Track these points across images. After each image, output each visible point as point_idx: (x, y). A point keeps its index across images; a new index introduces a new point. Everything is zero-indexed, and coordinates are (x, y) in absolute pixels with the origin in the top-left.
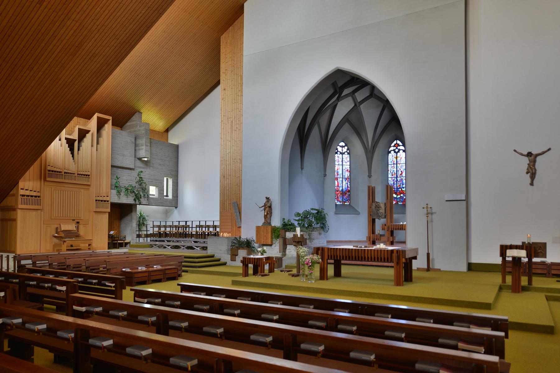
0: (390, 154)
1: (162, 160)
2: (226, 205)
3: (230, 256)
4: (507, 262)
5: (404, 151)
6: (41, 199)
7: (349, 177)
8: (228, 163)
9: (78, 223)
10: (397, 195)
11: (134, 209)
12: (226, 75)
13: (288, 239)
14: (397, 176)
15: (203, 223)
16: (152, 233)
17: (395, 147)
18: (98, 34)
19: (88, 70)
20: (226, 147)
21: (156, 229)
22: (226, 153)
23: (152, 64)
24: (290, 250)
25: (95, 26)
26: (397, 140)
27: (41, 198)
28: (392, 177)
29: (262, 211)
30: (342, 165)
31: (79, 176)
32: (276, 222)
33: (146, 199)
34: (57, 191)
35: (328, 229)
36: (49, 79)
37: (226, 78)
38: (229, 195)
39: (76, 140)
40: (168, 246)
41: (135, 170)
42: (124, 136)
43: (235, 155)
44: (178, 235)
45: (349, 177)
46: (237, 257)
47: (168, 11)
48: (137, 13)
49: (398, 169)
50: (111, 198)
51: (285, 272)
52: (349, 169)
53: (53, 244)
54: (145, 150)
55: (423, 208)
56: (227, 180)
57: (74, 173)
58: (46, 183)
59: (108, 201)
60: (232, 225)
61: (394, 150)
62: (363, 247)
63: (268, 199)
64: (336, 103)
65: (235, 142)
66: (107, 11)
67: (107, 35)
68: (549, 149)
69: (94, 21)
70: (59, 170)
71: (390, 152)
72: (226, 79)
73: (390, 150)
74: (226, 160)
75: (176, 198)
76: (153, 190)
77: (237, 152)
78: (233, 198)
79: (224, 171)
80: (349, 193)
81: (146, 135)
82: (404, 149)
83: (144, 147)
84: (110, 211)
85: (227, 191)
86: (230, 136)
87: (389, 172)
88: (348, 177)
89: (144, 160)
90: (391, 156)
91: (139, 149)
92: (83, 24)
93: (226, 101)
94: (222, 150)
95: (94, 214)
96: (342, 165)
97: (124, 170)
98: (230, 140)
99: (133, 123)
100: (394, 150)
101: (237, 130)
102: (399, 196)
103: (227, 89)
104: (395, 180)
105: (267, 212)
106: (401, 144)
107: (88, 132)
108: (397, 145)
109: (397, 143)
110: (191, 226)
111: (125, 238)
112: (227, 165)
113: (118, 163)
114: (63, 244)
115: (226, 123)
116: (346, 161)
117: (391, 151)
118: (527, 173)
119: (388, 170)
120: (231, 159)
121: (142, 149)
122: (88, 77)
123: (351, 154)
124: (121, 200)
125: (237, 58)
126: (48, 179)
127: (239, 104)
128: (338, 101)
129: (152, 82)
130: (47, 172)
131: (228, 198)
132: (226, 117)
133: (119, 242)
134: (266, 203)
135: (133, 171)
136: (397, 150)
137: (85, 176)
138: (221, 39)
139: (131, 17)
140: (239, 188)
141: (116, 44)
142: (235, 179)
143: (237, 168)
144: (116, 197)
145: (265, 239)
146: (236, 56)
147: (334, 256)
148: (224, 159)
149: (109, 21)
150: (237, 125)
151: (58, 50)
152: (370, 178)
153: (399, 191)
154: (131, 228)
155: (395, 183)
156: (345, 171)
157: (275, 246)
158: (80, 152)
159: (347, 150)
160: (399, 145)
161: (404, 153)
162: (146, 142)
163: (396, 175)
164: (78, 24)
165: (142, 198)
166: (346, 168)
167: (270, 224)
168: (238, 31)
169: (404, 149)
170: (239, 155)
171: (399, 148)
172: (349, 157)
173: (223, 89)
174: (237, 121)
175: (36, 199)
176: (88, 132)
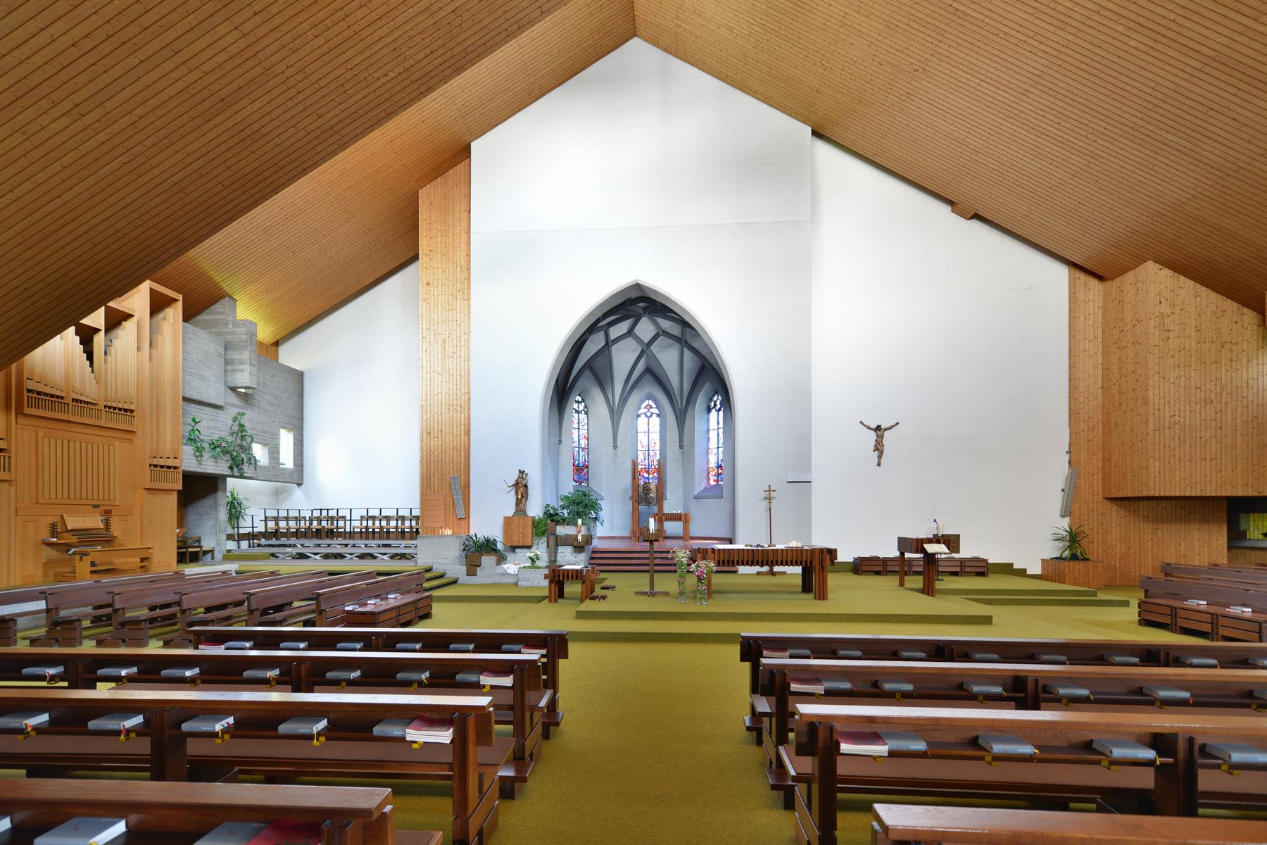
0: (639, 418)
1: (275, 396)
2: (434, 481)
5: (658, 415)
6: (9, 457)
9: (109, 512)
11: (220, 486)
12: (431, 259)
13: (560, 536)
15: (375, 513)
16: (263, 530)
18: (283, 87)
19: (229, 168)
21: (271, 524)
22: (432, 392)
23: (281, 207)
25: (282, 67)
26: (648, 399)
27: (10, 453)
29: (509, 492)
30: (578, 429)
31: (107, 409)
32: (535, 509)
33: (252, 468)
34: (53, 441)
36: (121, 158)
37: (432, 265)
39: (100, 330)
40: (316, 554)
41: (225, 410)
42: (203, 341)
43: (451, 399)
44: (348, 535)
47: (436, 92)
48: (378, 74)
50: (181, 462)
52: (586, 435)
53: (45, 560)
54: (250, 373)
55: (774, 491)
57: (95, 402)
58: (22, 420)
59: (175, 468)
60: (445, 516)
61: (645, 414)
63: (521, 472)
65: (451, 376)
66: (321, 40)
67: (301, 97)
68: (898, 424)
69: (285, 52)
70: (58, 393)
71: (639, 416)
72: (430, 266)
74: (432, 405)
75: (300, 468)
76: (259, 452)
77: (455, 393)
81: (250, 344)
83: (247, 367)
84: (181, 489)
86: (440, 365)
89: (240, 392)
90: (642, 422)
91: (235, 370)
92: (258, 49)
93: (432, 304)
94: (424, 389)
95: (144, 491)
96: (578, 429)
97: (203, 408)
98: (440, 372)
99: (217, 317)
100: (645, 414)
101: (455, 356)
103: (433, 283)
104: (647, 453)
105: (522, 494)
106: (654, 405)
107: (128, 316)
109: (648, 405)
110: (348, 518)
111: (199, 541)
112: (436, 414)
113: (191, 393)
114: (81, 560)
115: (432, 343)
116: (583, 424)
118: (874, 451)
121: (242, 370)
122: (221, 185)
123: (589, 413)
124: (201, 466)
125: (453, 234)
126: (27, 411)
129: (272, 243)
130: (26, 393)
131: (438, 470)
132: (432, 332)
133: (190, 550)
134: (520, 480)
135: (220, 412)
136: (649, 414)
137: (117, 411)
138: (420, 194)
139: (366, 76)
140: (459, 453)
141: (312, 127)
142: (451, 439)
143: (455, 421)
144: (194, 461)
146: (451, 231)
147: (806, 562)
148: (428, 403)
149: (317, 64)
150: (455, 348)
151: (172, 91)
154: (214, 523)
157: (537, 548)
158: (108, 357)
161: (658, 418)
162: (251, 359)
164: (242, 43)
165: (245, 464)
167: (525, 512)
168: (454, 189)
171: (651, 410)
173: (425, 282)
175: (4, 457)
176: (128, 316)
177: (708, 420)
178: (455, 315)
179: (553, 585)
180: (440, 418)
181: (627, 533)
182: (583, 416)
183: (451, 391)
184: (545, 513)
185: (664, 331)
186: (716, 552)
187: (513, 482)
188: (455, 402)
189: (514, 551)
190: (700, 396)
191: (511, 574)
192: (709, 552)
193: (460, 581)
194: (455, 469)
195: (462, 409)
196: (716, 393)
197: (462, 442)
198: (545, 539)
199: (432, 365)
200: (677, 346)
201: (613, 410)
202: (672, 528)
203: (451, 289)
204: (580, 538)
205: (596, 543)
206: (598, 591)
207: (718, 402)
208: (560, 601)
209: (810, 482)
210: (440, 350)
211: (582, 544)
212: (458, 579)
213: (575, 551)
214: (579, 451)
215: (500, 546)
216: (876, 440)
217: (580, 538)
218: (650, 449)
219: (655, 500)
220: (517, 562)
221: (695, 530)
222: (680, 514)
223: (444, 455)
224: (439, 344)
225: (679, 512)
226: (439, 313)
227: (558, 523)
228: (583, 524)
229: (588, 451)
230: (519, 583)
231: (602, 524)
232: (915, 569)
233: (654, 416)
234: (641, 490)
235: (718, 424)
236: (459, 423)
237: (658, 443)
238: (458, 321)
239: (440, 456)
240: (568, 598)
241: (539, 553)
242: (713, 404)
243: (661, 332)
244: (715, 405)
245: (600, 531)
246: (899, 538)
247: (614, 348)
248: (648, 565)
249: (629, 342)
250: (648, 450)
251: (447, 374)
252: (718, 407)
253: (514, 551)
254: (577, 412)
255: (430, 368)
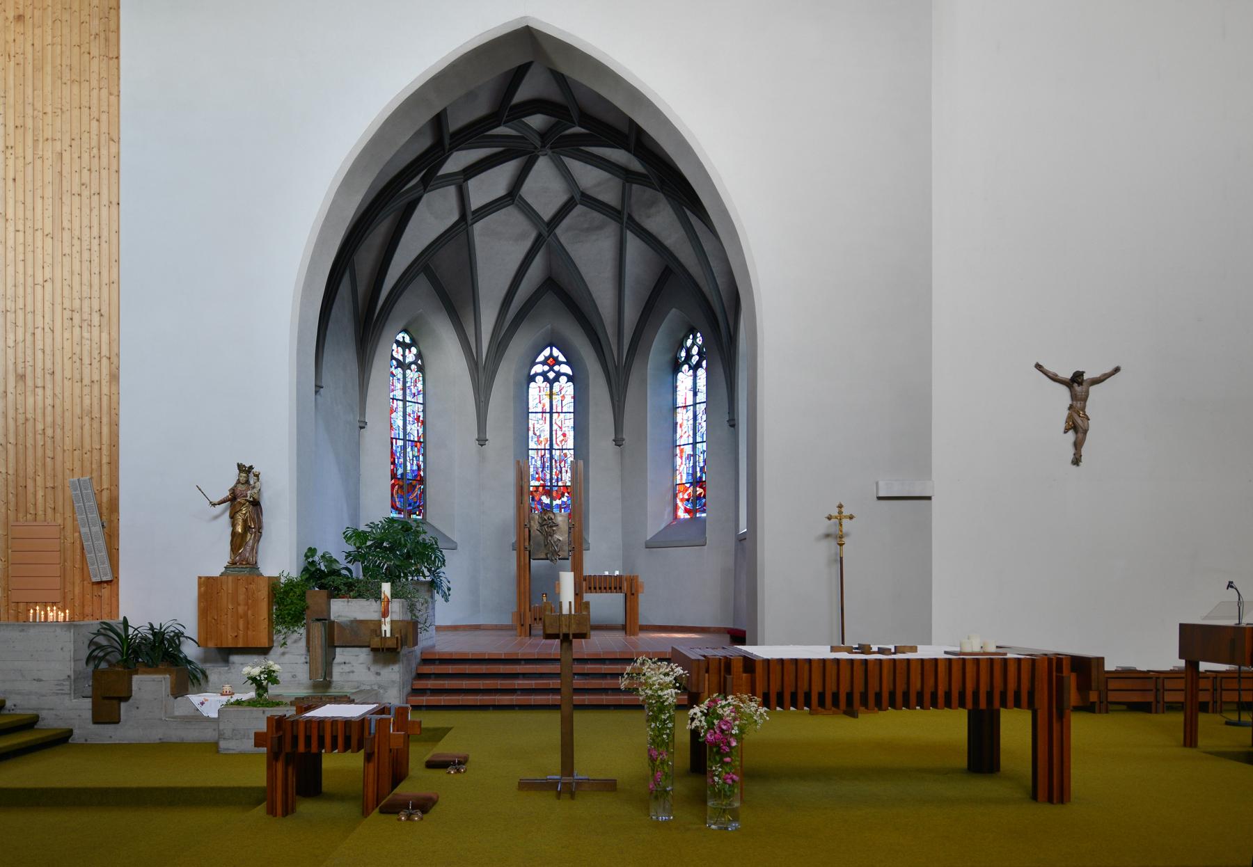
0: (532, 385)
3: (88, 703)
4: (1200, 675)
5: (570, 379)
7: (422, 440)
8: (39, 323)
10: (552, 499)
14: (551, 445)
17: (548, 365)
20: (29, 256)
22: (30, 280)
24: (347, 668)
26: (551, 345)
28: (539, 447)
29: (216, 517)
30: (404, 400)
35: (449, 589)
38: (50, 454)
43: (76, 295)
45: (422, 440)
46: (123, 705)
49: (555, 427)
51: (458, 771)
52: (421, 414)
55: (851, 517)
56: (40, 391)
61: (544, 374)
62: (875, 648)
63: (245, 470)
64: (416, 195)
65: (76, 242)
68: (1117, 370)
71: (532, 379)
73: (532, 372)
74: (29, 308)
78: (68, 465)
79: (20, 354)
80: (422, 487)
82: (569, 372)
85: (39, 437)
86: (48, 213)
87: (531, 433)
88: (419, 438)
90: (537, 392)
94: (10, 270)
98: (48, 229)
100: (544, 374)
101: (86, 193)
102: (558, 502)
103: (32, 17)
104: (548, 455)
105: (245, 521)
106: (562, 358)
108: (551, 359)
109: (551, 355)
112: (39, 332)
115: (29, 158)
116: (414, 390)
117: (537, 374)
119: (528, 429)
120: (58, 308)
127: (95, 93)
128: (425, 190)
131: (44, 465)
136: (551, 375)
140: (96, 425)
142: (77, 392)
143: (86, 348)
145: (241, 627)
147: (976, 694)
148: (20, 304)
150: (85, 172)
152: (482, 445)
153: (556, 488)
155: (548, 464)
156: (411, 419)
157: (283, 654)
159: (417, 359)
160: (560, 363)
163: (549, 442)
166: (413, 412)
167: (254, 567)
169: (569, 372)
170: (96, 294)
171: (556, 368)
172: (421, 379)
173: (11, 14)
174: (86, 156)
177: (675, 388)
178: (85, 92)
179: (280, 766)
180: (49, 341)
181: (507, 620)
182: (412, 374)
183: (76, 278)
184: (306, 570)
185: (583, 194)
186: (759, 670)
187: (226, 494)
188: (86, 303)
189: (226, 661)
190: (657, 336)
191: (208, 719)
192: (737, 667)
193: (78, 736)
194: (87, 464)
195: (105, 320)
196: (692, 331)
197: (105, 399)
198: (303, 631)
199: (29, 214)
200: (612, 228)
201: (476, 364)
202: (606, 606)
203: (76, 30)
204: (386, 628)
205: (430, 641)
206: (418, 782)
207: (695, 350)
208: (306, 807)
209: (929, 498)
210: (48, 178)
211: (392, 644)
212: (70, 732)
213: (376, 661)
214: (404, 448)
215: (190, 650)
216: (1071, 407)
217: (386, 628)
218: (555, 446)
219: (566, 548)
220: (227, 688)
221: (649, 612)
222: (620, 577)
223: (59, 431)
224: (48, 163)
225: (617, 573)
226: (48, 88)
227: (335, 593)
228: (395, 595)
229: (425, 448)
230: (223, 744)
231: (446, 597)
232: (1169, 697)
233: (563, 379)
234: (535, 526)
235: (695, 394)
236: (95, 353)
237: (571, 434)
238: (94, 109)
239: (49, 432)
240: (331, 797)
241: (276, 667)
242: (683, 354)
243: (577, 197)
244: (689, 356)
245: (444, 612)
246: (1181, 625)
247: (478, 228)
248: (556, 691)
249: (510, 217)
250: (551, 449)
251: (66, 235)
252: (695, 359)
253: (226, 661)
254: (402, 365)
255: (25, 219)
